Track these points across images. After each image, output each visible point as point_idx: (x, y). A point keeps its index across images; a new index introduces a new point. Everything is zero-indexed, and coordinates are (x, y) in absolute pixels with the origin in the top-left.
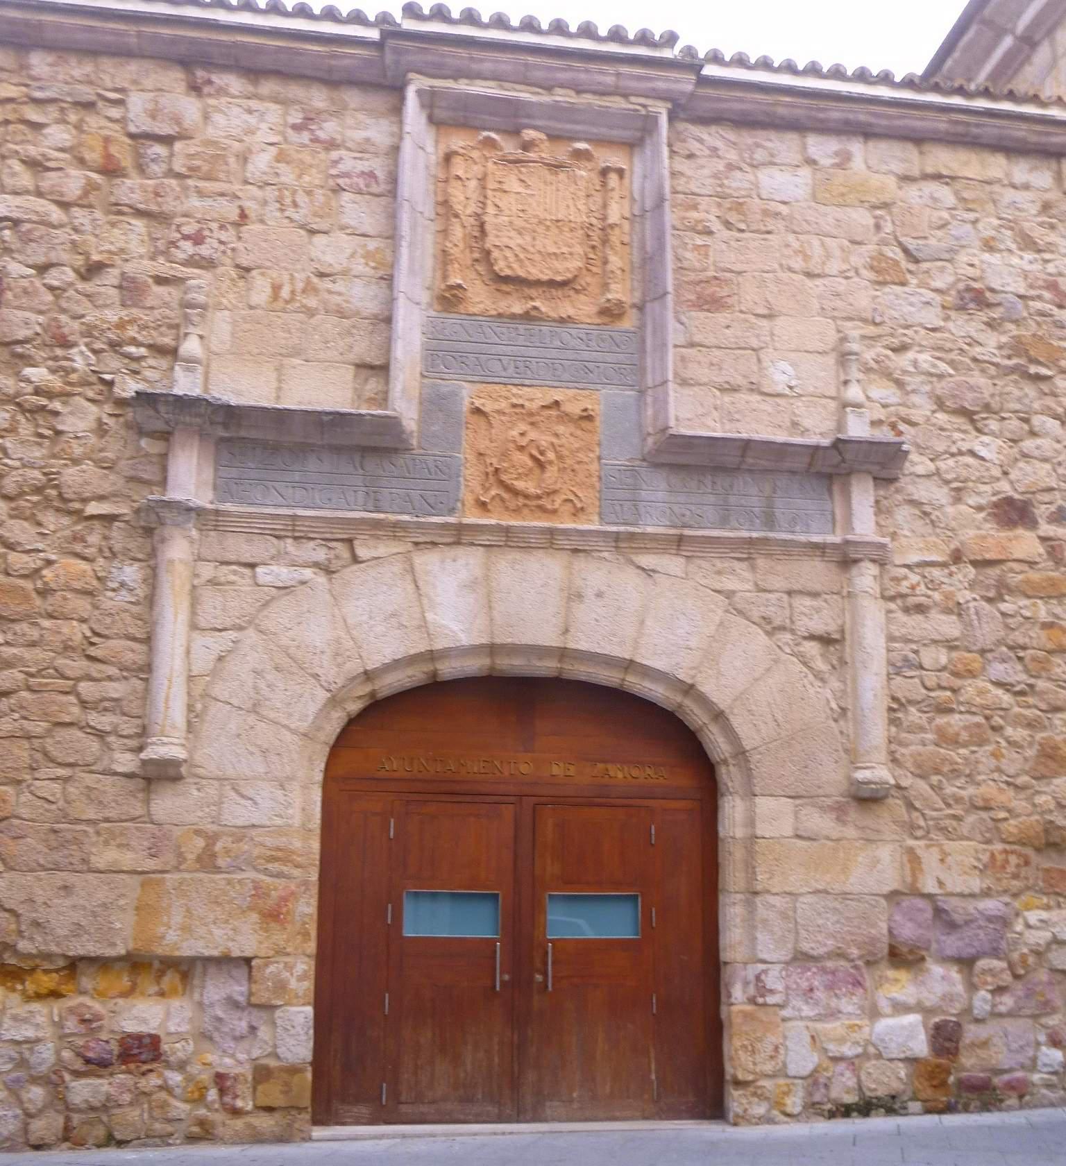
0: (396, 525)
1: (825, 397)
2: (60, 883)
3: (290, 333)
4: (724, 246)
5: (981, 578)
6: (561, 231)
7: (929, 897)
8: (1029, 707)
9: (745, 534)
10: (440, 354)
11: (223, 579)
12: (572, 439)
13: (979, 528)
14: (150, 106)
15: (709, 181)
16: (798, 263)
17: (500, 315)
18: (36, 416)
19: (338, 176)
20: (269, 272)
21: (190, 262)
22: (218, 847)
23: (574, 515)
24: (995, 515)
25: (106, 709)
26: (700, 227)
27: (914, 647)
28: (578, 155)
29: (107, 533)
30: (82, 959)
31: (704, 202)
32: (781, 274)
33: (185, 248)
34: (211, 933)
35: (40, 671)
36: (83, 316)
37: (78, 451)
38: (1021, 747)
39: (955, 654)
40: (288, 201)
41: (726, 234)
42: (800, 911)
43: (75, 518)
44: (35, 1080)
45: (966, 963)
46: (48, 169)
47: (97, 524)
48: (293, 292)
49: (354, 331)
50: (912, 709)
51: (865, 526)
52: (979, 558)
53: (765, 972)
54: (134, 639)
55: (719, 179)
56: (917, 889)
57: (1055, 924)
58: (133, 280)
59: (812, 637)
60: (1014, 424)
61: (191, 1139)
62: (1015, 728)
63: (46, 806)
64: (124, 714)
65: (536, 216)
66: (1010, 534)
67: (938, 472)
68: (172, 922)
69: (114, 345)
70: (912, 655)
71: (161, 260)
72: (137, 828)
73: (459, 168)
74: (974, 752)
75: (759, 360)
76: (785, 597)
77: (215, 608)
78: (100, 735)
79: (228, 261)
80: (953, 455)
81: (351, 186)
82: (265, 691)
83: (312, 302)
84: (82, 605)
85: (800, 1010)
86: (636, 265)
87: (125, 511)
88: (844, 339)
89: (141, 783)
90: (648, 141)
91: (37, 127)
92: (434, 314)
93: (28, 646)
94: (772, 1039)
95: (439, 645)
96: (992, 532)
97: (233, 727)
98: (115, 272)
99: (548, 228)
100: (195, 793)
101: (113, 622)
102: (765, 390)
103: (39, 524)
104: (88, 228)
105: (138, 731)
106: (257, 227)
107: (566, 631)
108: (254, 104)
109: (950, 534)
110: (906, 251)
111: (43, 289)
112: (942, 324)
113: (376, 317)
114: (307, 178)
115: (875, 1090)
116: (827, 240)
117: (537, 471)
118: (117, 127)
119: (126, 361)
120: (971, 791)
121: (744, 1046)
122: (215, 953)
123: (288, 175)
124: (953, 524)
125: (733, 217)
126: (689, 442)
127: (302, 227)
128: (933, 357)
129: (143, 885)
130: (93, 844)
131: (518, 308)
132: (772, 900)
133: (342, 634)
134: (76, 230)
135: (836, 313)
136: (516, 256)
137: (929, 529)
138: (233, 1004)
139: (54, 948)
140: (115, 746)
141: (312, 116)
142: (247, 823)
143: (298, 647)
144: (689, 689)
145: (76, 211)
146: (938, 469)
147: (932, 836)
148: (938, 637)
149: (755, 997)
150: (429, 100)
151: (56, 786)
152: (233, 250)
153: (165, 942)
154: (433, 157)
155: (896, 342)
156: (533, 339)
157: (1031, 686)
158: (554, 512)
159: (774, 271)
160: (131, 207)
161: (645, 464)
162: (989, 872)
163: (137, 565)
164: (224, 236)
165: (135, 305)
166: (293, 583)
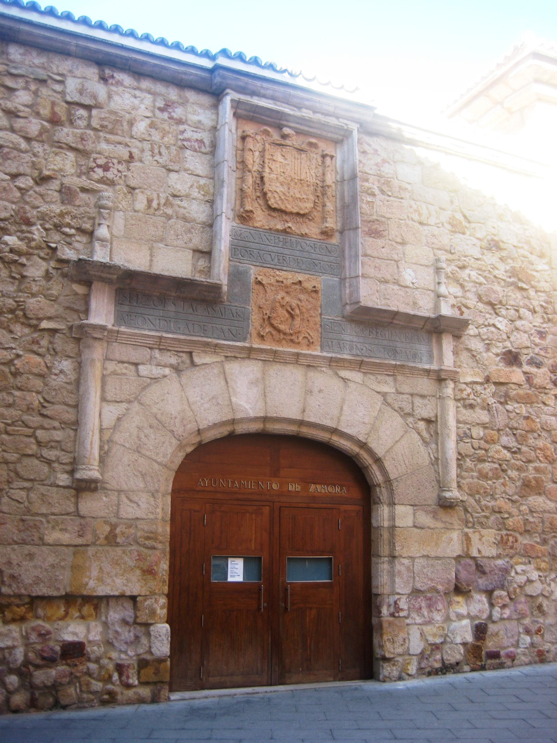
0: (216, 345)
1: (429, 290)
2: (26, 552)
3: (157, 228)
4: (381, 203)
5: (497, 391)
6: (303, 186)
7: (474, 558)
8: (518, 460)
9: (394, 363)
10: (239, 248)
11: (119, 372)
12: (307, 303)
13: (497, 366)
14: (79, 87)
15: (374, 167)
16: (416, 217)
17: (270, 229)
18: (11, 266)
19: (183, 140)
20: (146, 191)
21: (101, 181)
22: (118, 531)
23: (308, 346)
24: (504, 359)
25: (52, 447)
26: (369, 192)
27: (469, 426)
28: (311, 144)
29: (52, 340)
30: (37, 597)
31: (371, 178)
32: (407, 221)
33: (98, 172)
34: (114, 581)
35: (13, 422)
36: (38, 207)
37: (35, 289)
38: (514, 480)
39: (486, 431)
40: (156, 151)
41: (382, 197)
42: (415, 566)
43: (32, 329)
44: (11, 671)
45: (489, 593)
46: (19, 117)
47: (46, 334)
48: (159, 204)
49: (193, 230)
50: (468, 460)
51: (449, 361)
52: (497, 381)
53: (399, 599)
54: (68, 405)
55: (379, 167)
56: (469, 554)
57: (528, 572)
58: (69, 189)
59: (423, 419)
60: (512, 312)
61: (104, 703)
62: (512, 471)
63: (18, 505)
64: (63, 450)
65: (290, 176)
66: (511, 369)
67: (479, 335)
68: (92, 575)
69: (57, 227)
70: (468, 431)
71: (84, 178)
72: (71, 519)
73: (250, 143)
74: (494, 483)
75: (398, 267)
76: (410, 397)
77: (116, 389)
78: (49, 462)
79: (121, 182)
80: (486, 326)
81: (191, 146)
82: (144, 439)
83: (169, 211)
84: (38, 383)
85: (414, 619)
86: (338, 208)
87: (64, 327)
88: (438, 260)
89: (73, 492)
90: (345, 142)
91: (11, 90)
92: (236, 225)
93: (6, 406)
94: (402, 635)
95: (239, 416)
96: (503, 368)
97: (125, 460)
98: (58, 182)
99: (296, 184)
100: (104, 499)
101: (56, 394)
102: (401, 284)
103: (11, 332)
104: (41, 154)
105: (72, 460)
106: (138, 164)
107: (304, 411)
108: (137, 93)
109: (484, 367)
110: (465, 217)
111: (15, 189)
112: (481, 256)
113: (204, 223)
114: (166, 139)
115: (449, 660)
116: (429, 206)
117: (290, 320)
118: (59, 96)
119: (64, 236)
120: (493, 503)
121: (388, 639)
122: (117, 593)
123: (156, 136)
124: (486, 362)
125: (385, 188)
126: (368, 310)
127: (164, 167)
128: (477, 273)
129: (74, 554)
130: (46, 529)
131: (280, 227)
132: (403, 560)
133: (186, 407)
134: (35, 155)
135: (433, 246)
136: (280, 197)
137: (475, 364)
138: (125, 622)
139: (23, 591)
140: (57, 470)
141: (170, 104)
142: (134, 517)
143: (162, 414)
144: (363, 445)
145: (35, 144)
146: (479, 333)
147: (475, 526)
148: (479, 422)
149: (394, 613)
150: (236, 104)
151: (23, 494)
152: (125, 176)
153: (88, 587)
154: (235, 136)
155: (461, 264)
156: (287, 244)
157: (519, 449)
158: (299, 343)
159: (405, 220)
160: (67, 144)
161: (344, 320)
162: (500, 546)
163: (70, 360)
164: (120, 168)
165: (69, 204)
166: (159, 376)
